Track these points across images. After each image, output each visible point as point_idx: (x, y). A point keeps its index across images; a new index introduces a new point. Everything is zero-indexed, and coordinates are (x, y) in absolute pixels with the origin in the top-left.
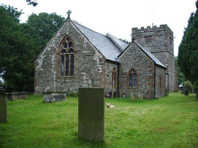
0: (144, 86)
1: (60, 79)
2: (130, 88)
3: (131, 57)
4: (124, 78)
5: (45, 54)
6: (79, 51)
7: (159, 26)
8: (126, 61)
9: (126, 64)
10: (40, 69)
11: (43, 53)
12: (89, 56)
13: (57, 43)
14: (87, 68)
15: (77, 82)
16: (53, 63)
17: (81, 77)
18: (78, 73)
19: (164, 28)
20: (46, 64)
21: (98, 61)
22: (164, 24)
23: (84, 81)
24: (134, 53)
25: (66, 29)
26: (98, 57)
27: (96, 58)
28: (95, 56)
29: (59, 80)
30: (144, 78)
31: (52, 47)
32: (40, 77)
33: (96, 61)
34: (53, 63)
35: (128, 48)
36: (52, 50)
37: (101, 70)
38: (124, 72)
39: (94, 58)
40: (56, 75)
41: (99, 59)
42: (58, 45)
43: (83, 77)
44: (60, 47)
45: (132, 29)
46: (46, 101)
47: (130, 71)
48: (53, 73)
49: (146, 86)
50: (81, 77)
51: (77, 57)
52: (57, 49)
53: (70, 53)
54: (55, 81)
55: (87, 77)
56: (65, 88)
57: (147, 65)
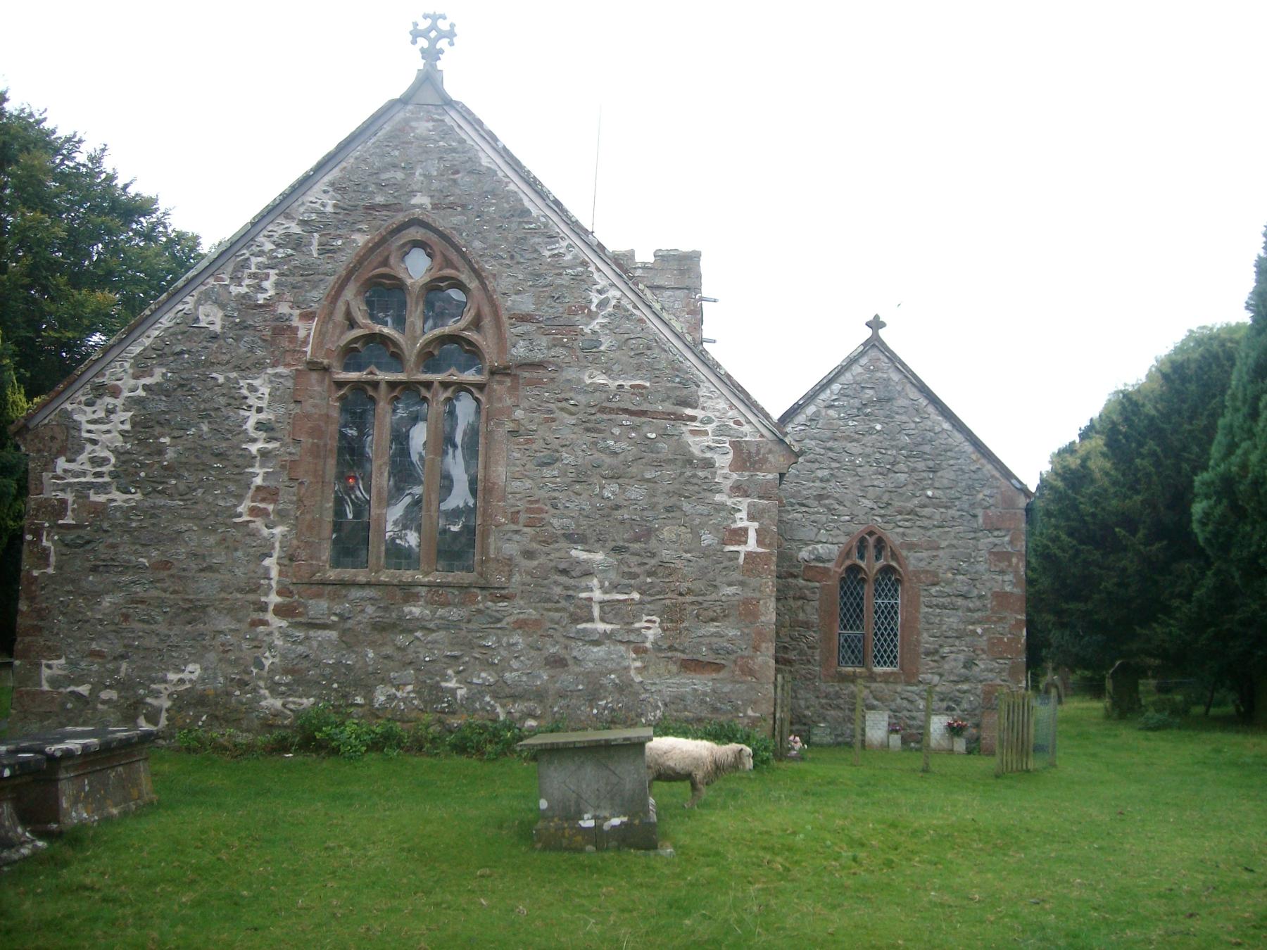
0: (781, 654)
1: (334, 597)
2: (852, 678)
3: (854, 447)
4: (803, 598)
5: (160, 353)
6: (540, 365)
7: (651, 259)
8: (820, 474)
9: (820, 497)
10: (102, 488)
11: (137, 349)
12: (643, 413)
13: (308, 274)
14: (624, 514)
15: (521, 625)
16: (254, 448)
17: (558, 590)
18: (529, 555)
19: (682, 272)
20: (170, 454)
21: (723, 461)
22: (685, 247)
23: (591, 620)
24: (878, 427)
25: (409, 169)
26: (722, 430)
27: (708, 441)
28: (693, 419)
29: (319, 607)
30: (960, 601)
31: (246, 303)
32: (95, 569)
33: (708, 464)
34: (254, 448)
35: (836, 387)
36: (243, 327)
37: (752, 536)
38: (804, 554)
39: (690, 439)
40: (290, 558)
41: (736, 445)
42: (316, 296)
43: (584, 582)
44: (339, 316)
45: (197, 237)
46: (588, 823)
47: (848, 554)
48: (254, 534)
49: (969, 664)
50: (558, 590)
51: (519, 414)
52: (307, 330)
53: (439, 377)
54: (280, 611)
55: (615, 587)
56: (384, 681)
57: (979, 512)
